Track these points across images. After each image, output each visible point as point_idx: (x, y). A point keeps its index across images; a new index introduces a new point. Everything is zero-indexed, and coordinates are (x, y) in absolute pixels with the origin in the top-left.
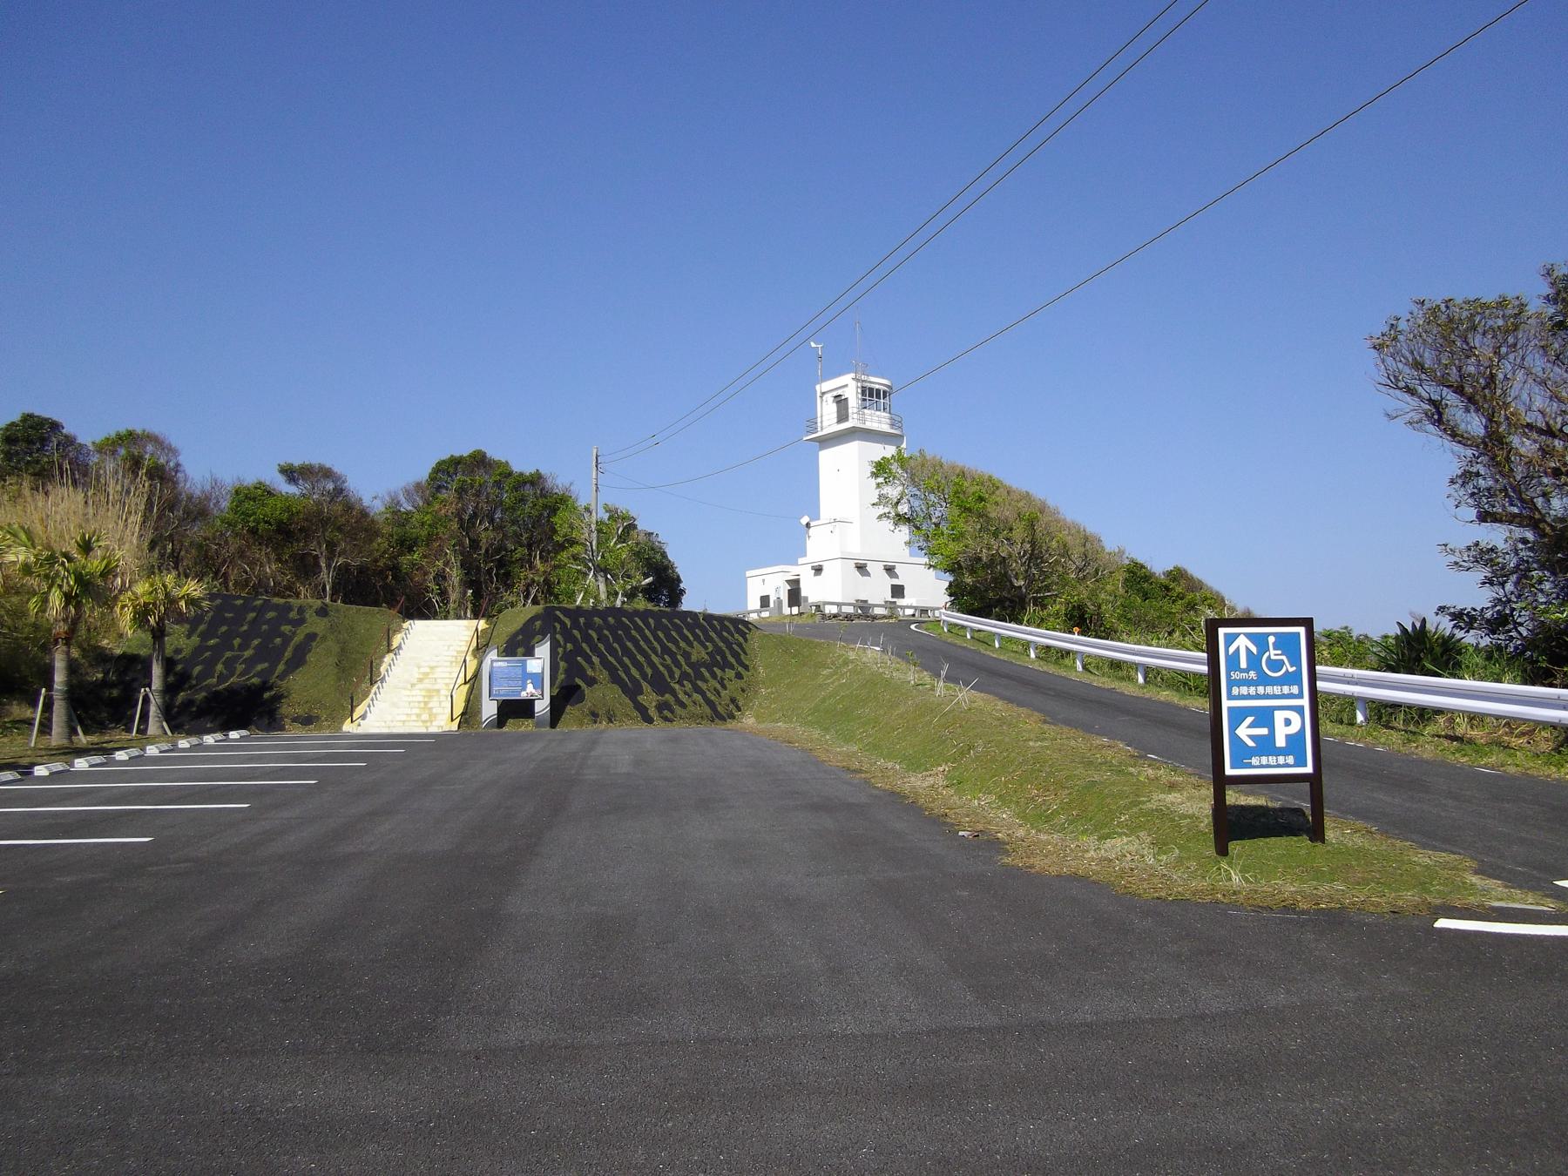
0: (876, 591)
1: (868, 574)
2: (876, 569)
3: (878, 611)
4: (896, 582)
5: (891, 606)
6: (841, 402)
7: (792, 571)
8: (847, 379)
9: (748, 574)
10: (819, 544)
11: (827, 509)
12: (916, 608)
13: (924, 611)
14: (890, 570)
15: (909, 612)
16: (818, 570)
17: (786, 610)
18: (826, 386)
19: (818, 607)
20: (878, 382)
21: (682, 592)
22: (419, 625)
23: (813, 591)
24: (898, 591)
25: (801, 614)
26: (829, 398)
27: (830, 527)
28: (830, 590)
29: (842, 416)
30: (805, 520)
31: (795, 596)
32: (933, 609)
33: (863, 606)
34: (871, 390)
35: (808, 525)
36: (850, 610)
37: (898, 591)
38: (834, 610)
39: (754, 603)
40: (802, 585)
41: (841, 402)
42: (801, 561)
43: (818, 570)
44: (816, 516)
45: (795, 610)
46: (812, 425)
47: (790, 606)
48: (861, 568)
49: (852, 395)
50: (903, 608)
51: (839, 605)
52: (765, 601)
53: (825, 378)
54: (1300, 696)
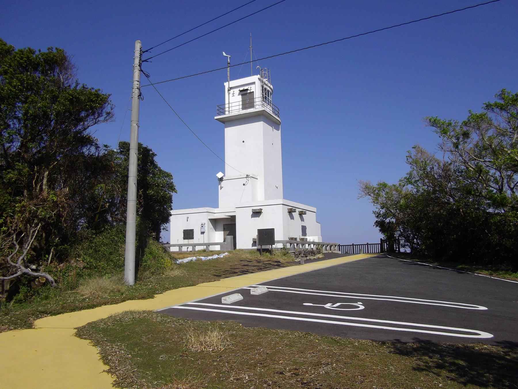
4: (304, 224)
8: (255, 78)
18: (234, 83)
26: (237, 91)
37: (304, 229)
41: (246, 95)
46: (222, 110)
49: (257, 90)
53: (233, 78)
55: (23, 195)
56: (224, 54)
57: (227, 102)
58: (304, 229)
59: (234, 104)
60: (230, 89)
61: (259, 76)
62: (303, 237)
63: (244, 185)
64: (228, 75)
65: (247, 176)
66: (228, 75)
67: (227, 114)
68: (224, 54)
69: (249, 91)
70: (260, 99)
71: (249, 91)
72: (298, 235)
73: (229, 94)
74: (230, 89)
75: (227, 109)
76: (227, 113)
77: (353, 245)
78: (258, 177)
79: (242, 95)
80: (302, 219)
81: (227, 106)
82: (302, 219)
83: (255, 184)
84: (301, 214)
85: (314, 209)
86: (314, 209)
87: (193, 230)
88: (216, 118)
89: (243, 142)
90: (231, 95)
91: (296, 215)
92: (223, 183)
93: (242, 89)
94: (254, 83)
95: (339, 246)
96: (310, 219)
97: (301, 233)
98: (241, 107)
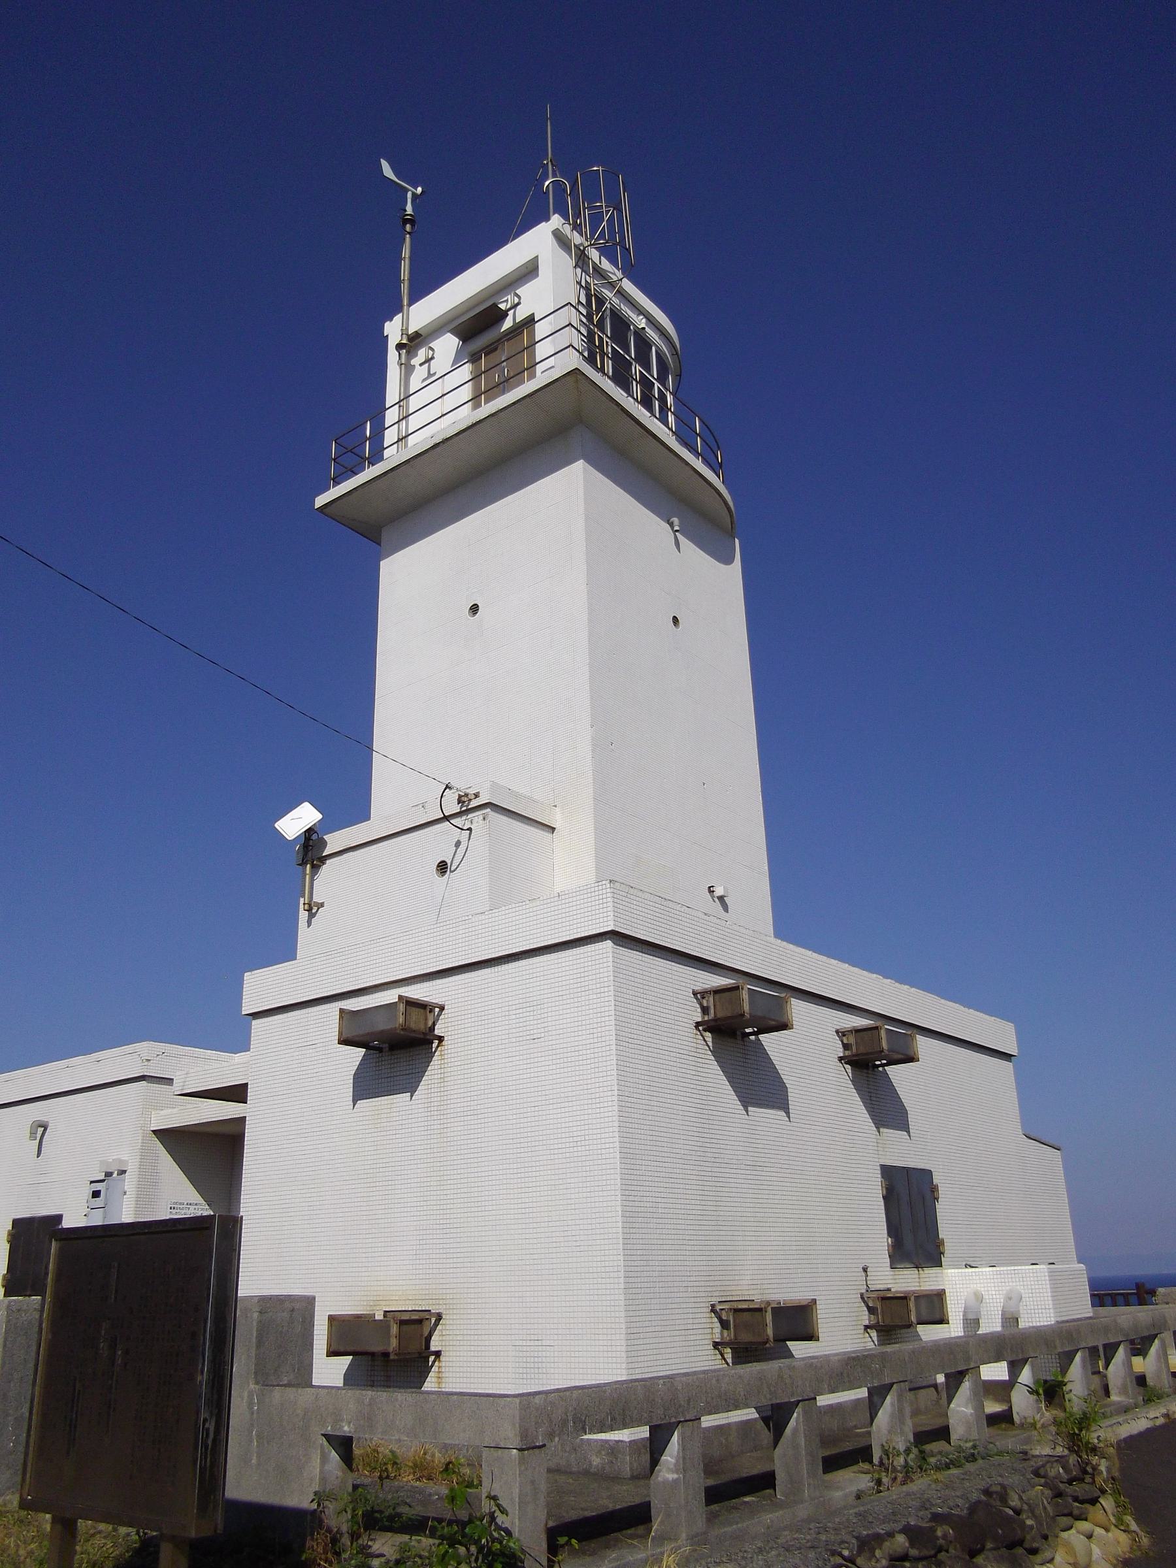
4: (901, 1150)
8: (538, 242)
16: (395, 1046)
26: (447, 345)
30: (298, 820)
35: (311, 850)
37: (911, 1213)
42: (261, 987)
43: (395, 1046)
44: (349, 799)
53: (417, 295)
55: (871, 1462)
56: (387, 171)
57: (392, 394)
58: (911, 1213)
59: (430, 401)
60: (413, 342)
62: (908, 1281)
63: (442, 867)
65: (467, 806)
67: (393, 456)
68: (387, 171)
69: (508, 324)
71: (508, 324)
72: (834, 1265)
73: (407, 369)
74: (413, 342)
78: (557, 821)
80: (887, 1111)
81: (391, 416)
82: (887, 1111)
84: (872, 1056)
85: (1002, 1035)
86: (1002, 1035)
87: (887, 1172)
88: (320, 501)
89: (474, 609)
90: (419, 373)
91: (806, 1050)
92: (328, 883)
94: (542, 272)
96: (965, 1109)
97: (881, 1241)
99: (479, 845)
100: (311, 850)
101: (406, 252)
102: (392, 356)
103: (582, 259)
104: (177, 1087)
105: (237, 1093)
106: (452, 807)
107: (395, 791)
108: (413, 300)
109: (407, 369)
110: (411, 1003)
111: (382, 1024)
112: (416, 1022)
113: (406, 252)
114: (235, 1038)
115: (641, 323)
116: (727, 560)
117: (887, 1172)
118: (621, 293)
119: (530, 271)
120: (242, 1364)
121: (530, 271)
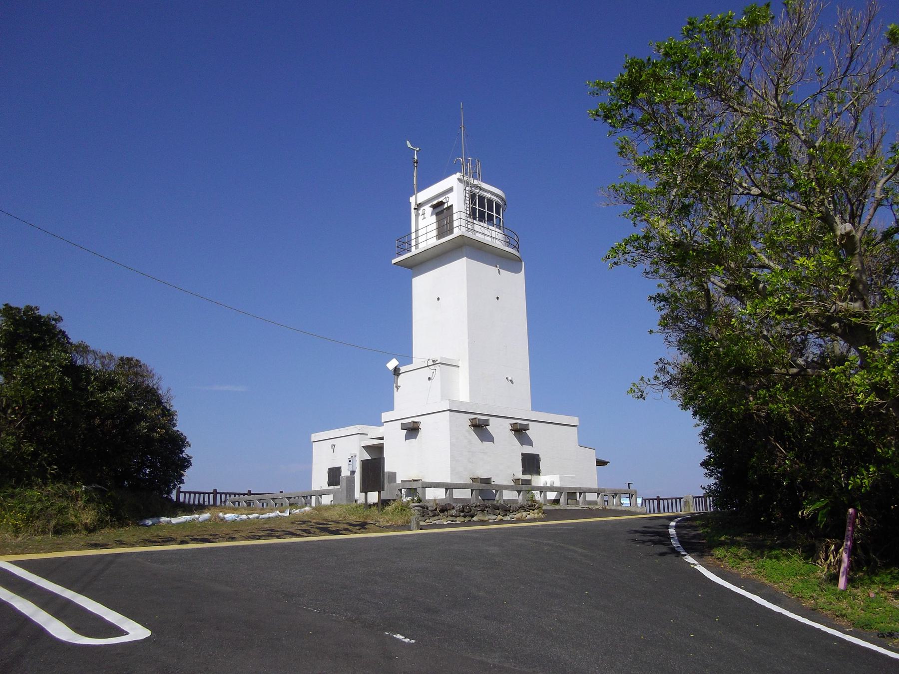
0: (501, 463)
1: (651, 298)
2: (500, 429)
3: (508, 495)
4: (528, 450)
5: (523, 486)
6: (442, 211)
7: (374, 432)
8: (452, 181)
9: (314, 437)
10: (412, 395)
11: (424, 345)
12: (560, 490)
13: (571, 494)
14: (520, 431)
15: (551, 496)
16: (412, 430)
17: (359, 495)
18: (423, 196)
19: (412, 491)
20: (492, 191)
21: (185, 463)
22: (388, 468)
23: (402, 463)
24: (531, 464)
25: (384, 503)
26: (428, 209)
27: (428, 372)
28: (429, 462)
29: (444, 227)
30: (392, 364)
31: (373, 471)
32: (583, 492)
33: (484, 487)
34: (481, 198)
35: (396, 372)
36: (465, 494)
37: (531, 464)
38: (439, 494)
39: (320, 481)
40: (386, 454)
41: (442, 211)
42: (385, 416)
43: (412, 430)
44: (406, 357)
45: (373, 497)
46: (405, 245)
47: (365, 489)
48: (480, 427)
49: (457, 201)
50: (543, 490)
51: (448, 487)
52: (334, 475)
53: (421, 188)
54: (659, 511)
56: (409, 145)
57: (413, 230)
59: (425, 232)
60: (419, 206)
61: (458, 175)
64: (415, 182)
66: (415, 182)
67: (414, 251)
68: (409, 145)
69: (446, 206)
70: (463, 216)
71: (446, 206)
73: (417, 215)
74: (419, 206)
75: (413, 243)
76: (413, 249)
77: (658, 499)
79: (437, 214)
81: (413, 236)
83: (471, 376)
85: (575, 421)
86: (575, 421)
87: (522, 454)
88: (394, 261)
90: (421, 217)
92: (401, 380)
93: (435, 202)
94: (453, 189)
95: (658, 499)
98: (435, 233)
99: (438, 373)
100: (396, 372)
101: (415, 174)
102: (413, 211)
103: (467, 184)
104: (370, 436)
105: (382, 438)
106: (431, 363)
107: (417, 361)
108: (419, 191)
109: (417, 215)
110: (414, 422)
111: (409, 426)
112: (415, 426)
113: (415, 174)
114: (381, 424)
115: (489, 196)
116: (517, 271)
117: (522, 454)
118: (481, 189)
119: (450, 190)
120: (386, 481)
121: (450, 190)
